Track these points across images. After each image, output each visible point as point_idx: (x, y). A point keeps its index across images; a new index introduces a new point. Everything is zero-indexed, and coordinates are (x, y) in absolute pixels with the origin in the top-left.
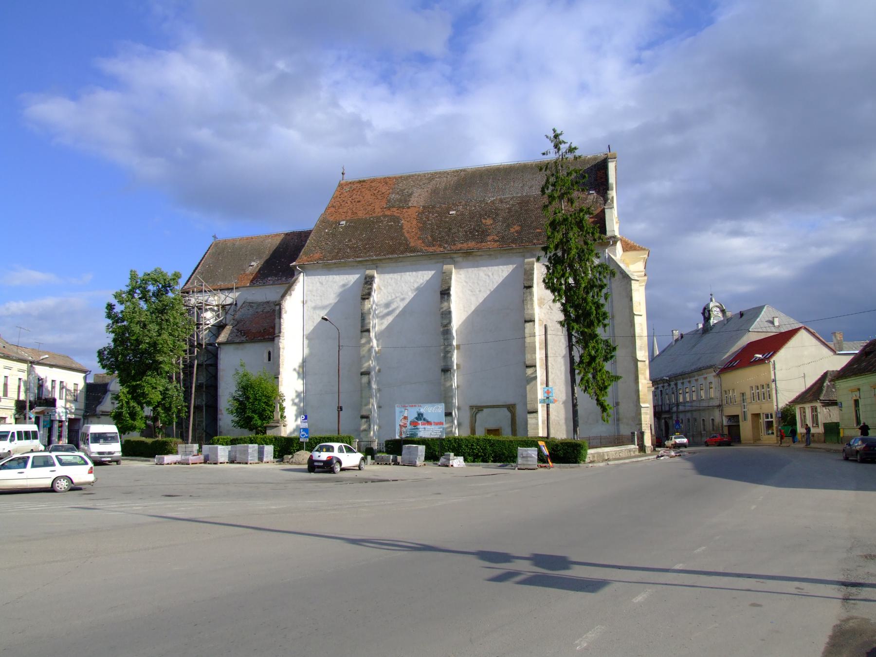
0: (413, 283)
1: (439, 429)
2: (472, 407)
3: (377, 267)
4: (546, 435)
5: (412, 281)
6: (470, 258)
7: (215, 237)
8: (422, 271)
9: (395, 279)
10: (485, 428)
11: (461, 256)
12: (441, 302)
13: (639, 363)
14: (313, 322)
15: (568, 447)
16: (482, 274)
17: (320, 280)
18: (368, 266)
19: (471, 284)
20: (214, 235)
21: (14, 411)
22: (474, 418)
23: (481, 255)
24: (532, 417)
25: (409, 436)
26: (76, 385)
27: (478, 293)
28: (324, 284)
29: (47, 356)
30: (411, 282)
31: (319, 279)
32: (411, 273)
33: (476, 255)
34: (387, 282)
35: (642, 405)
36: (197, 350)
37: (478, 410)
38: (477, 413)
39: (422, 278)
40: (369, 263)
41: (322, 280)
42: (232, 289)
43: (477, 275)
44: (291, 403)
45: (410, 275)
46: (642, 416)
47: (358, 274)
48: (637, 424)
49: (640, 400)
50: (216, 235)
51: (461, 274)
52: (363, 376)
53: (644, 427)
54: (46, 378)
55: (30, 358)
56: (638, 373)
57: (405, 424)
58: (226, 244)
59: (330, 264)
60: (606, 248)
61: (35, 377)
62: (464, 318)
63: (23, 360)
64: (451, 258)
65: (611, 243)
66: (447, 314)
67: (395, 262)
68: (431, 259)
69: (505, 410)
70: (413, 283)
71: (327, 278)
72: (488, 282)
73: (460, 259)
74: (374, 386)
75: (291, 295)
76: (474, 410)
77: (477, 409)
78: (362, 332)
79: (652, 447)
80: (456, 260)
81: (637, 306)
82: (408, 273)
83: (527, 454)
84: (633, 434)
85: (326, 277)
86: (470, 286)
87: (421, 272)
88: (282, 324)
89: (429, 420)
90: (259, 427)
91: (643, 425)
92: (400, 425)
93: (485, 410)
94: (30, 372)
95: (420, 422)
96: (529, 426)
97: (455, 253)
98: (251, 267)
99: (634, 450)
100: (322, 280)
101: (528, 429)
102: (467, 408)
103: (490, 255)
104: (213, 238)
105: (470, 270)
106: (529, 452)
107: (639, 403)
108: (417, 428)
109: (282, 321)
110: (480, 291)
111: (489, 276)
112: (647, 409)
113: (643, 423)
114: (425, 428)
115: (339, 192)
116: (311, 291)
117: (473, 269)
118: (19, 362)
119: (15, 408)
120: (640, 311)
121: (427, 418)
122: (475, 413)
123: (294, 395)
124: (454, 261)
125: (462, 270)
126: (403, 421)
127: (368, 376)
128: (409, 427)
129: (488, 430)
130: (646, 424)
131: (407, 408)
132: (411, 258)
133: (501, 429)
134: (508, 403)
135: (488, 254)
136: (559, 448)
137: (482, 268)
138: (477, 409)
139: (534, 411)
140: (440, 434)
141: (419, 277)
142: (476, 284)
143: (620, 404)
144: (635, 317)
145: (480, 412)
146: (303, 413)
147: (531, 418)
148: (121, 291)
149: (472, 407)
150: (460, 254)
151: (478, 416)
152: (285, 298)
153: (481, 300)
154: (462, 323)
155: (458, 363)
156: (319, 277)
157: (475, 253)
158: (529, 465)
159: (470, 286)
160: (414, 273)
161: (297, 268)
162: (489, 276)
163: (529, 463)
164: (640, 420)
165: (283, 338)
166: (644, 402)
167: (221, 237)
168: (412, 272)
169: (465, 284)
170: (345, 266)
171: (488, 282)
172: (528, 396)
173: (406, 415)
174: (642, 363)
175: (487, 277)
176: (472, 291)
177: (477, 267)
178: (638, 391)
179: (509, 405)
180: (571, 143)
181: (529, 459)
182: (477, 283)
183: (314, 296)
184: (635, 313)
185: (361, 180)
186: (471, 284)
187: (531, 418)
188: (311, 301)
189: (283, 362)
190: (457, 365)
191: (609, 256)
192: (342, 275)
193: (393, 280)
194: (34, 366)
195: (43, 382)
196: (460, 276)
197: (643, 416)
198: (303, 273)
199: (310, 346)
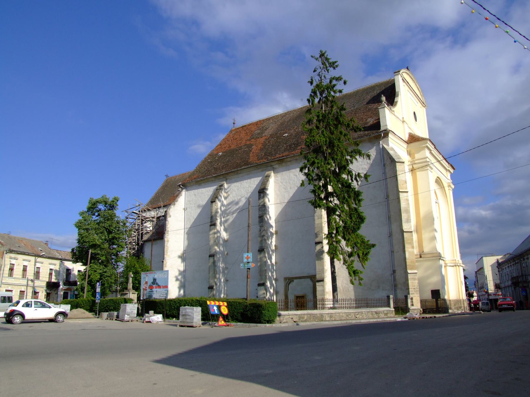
0: (248, 188)
1: (165, 292)
2: (285, 279)
3: (226, 179)
4: (26, 286)
5: (247, 186)
6: (284, 164)
7: (167, 176)
8: (253, 178)
9: (237, 186)
10: (295, 295)
11: (277, 164)
12: (259, 199)
13: (405, 234)
14: (190, 222)
15: (254, 307)
16: (292, 175)
17: (195, 193)
18: (221, 179)
19: (284, 184)
20: (166, 175)
21: (45, 288)
22: (287, 287)
23: (290, 161)
24: (320, 285)
25: (147, 297)
26: (39, 269)
27: (289, 189)
28: (196, 195)
29: (44, 253)
30: (246, 188)
31: (194, 192)
32: (247, 180)
33: (287, 161)
34: (233, 189)
35: (409, 271)
36: (137, 247)
37: (291, 281)
38: (289, 283)
39: (253, 183)
40: (222, 177)
41: (195, 193)
42: (161, 207)
43: (289, 176)
44: (175, 279)
45: (246, 182)
46: (409, 281)
47: (215, 186)
48: (407, 289)
49: (407, 267)
50: (168, 175)
51: (278, 177)
52: (210, 258)
53: (411, 291)
54: (73, 268)
55: (60, 257)
56: (404, 243)
57: (146, 288)
58: (172, 179)
59: (199, 181)
60: (380, 140)
61: (65, 268)
62: (280, 210)
63: (53, 258)
64: (271, 166)
65: (382, 135)
66: (263, 209)
67: (236, 175)
68: (258, 169)
69: (309, 280)
70: (248, 188)
71: (198, 191)
72: (296, 180)
73: (276, 166)
74: (221, 265)
75: (175, 204)
76: (287, 281)
77: (289, 280)
78: (211, 225)
79: (421, 310)
80: (275, 166)
81: (403, 184)
82: (245, 181)
83: (185, 312)
84: (388, 297)
85: (198, 191)
86: (284, 185)
87: (253, 179)
88: (167, 224)
89: (160, 284)
90: (266, 299)
91: (410, 290)
92: (143, 288)
93: (295, 281)
94: (61, 264)
95: (154, 286)
96: (317, 293)
97: (272, 162)
98: (178, 192)
99: (386, 312)
100: (195, 193)
101: (317, 295)
102: (282, 280)
103: (296, 160)
104: (166, 177)
105: (284, 173)
106: (188, 310)
107: (406, 270)
108: (152, 291)
109: (167, 222)
110: (291, 188)
111: (296, 176)
112: (415, 274)
113: (410, 287)
114: (157, 291)
115: (251, 141)
116: (189, 201)
117: (286, 172)
118: (49, 259)
119: (46, 287)
120: (406, 188)
121: (158, 283)
122: (288, 283)
123: (177, 273)
124: (273, 168)
125: (279, 173)
126: (145, 285)
127: (213, 257)
128: (148, 290)
129: (297, 297)
130: (414, 289)
131: (148, 275)
132: (245, 170)
133: (306, 296)
134: (310, 275)
135: (295, 159)
136: (248, 309)
137: (292, 170)
138: (289, 280)
139: (321, 280)
140: (165, 295)
141: (252, 183)
142: (288, 183)
143: (397, 272)
144: (401, 194)
145: (292, 282)
146: (182, 286)
147: (319, 286)
148: (83, 211)
149: (285, 279)
150: (276, 162)
151: (290, 285)
152: (170, 206)
153: (291, 195)
154: (279, 214)
155: (276, 245)
156: (194, 191)
157: (285, 160)
158: (188, 322)
159: (284, 185)
160: (249, 180)
161: (181, 186)
162: (296, 176)
163: (188, 321)
164: (408, 285)
165: (168, 234)
166: (411, 269)
167: (170, 175)
168: (247, 179)
169: (281, 184)
170: (208, 182)
171: (296, 180)
172: (317, 267)
173: (146, 280)
174: (409, 234)
175: (295, 177)
176: (285, 189)
177: (289, 170)
178: (405, 259)
179: (311, 276)
180: (331, 59)
181: (188, 317)
182: (289, 182)
183: (191, 204)
184: (400, 190)
185: (243, 125)
186: (284, 184)
187: (319, 286)
188: (189, 208)
189: (167, 251)
190: (275, 246)
191: (383, 146)
192: (206, 187)
193: (236, 187)
194: (63, 261)
195: (71, 271)
196: (277, 178)
197: (410, 281)
198: (185, 189)
199: (189, 239)
